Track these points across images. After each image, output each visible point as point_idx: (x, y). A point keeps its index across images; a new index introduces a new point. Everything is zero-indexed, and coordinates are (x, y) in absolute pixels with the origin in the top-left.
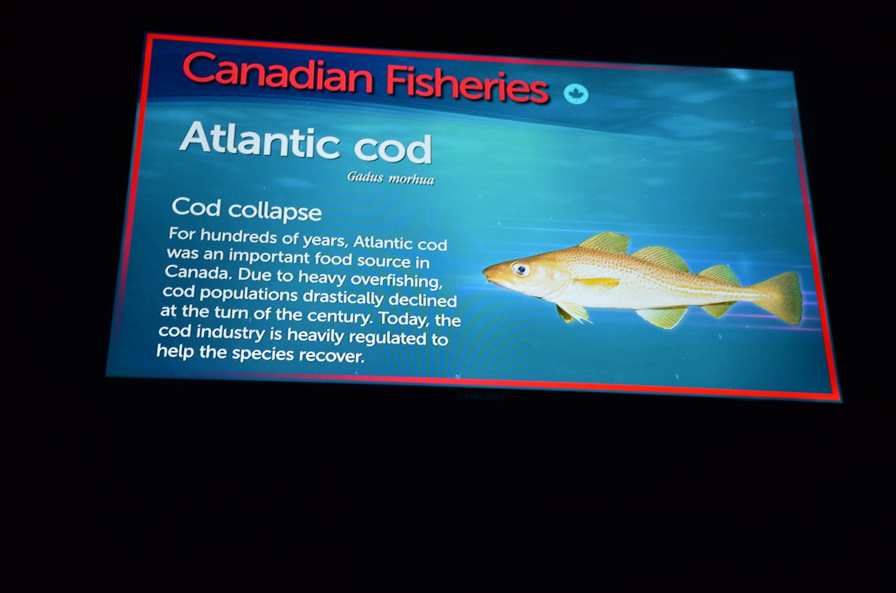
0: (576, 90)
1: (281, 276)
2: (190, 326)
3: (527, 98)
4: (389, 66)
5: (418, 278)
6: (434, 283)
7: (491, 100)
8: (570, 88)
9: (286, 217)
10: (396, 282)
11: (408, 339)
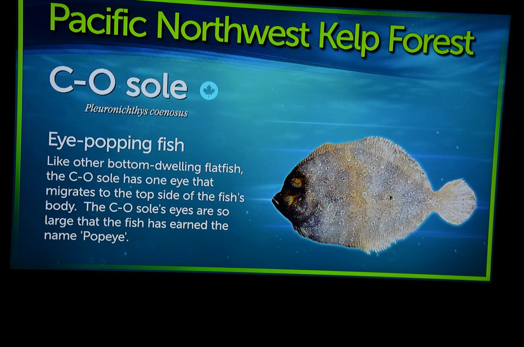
0: (209, 87)
1: (139, 194)
4: (52, 4)
6: (198, 168)
11: (84, 192)
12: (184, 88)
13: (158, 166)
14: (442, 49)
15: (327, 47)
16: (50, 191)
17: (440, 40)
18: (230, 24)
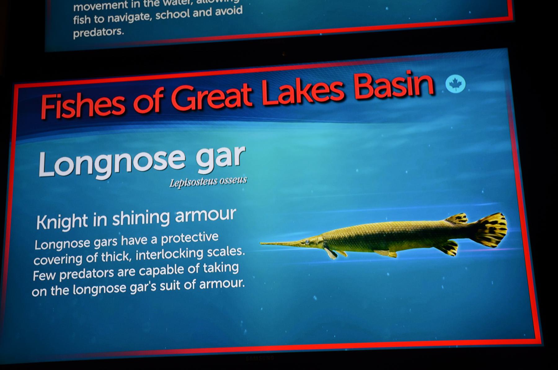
0: (455, 80)
2: (211, 8)
3: (327, 98)
7: (301, 103)
8: (450, 79)
9: (84, 273)
10: (80, 21)
12: (182, 158)
14: (320, 96)
15: (305, 101)
16: (77, 8)
17: (214, 95)
18: (82, 99)
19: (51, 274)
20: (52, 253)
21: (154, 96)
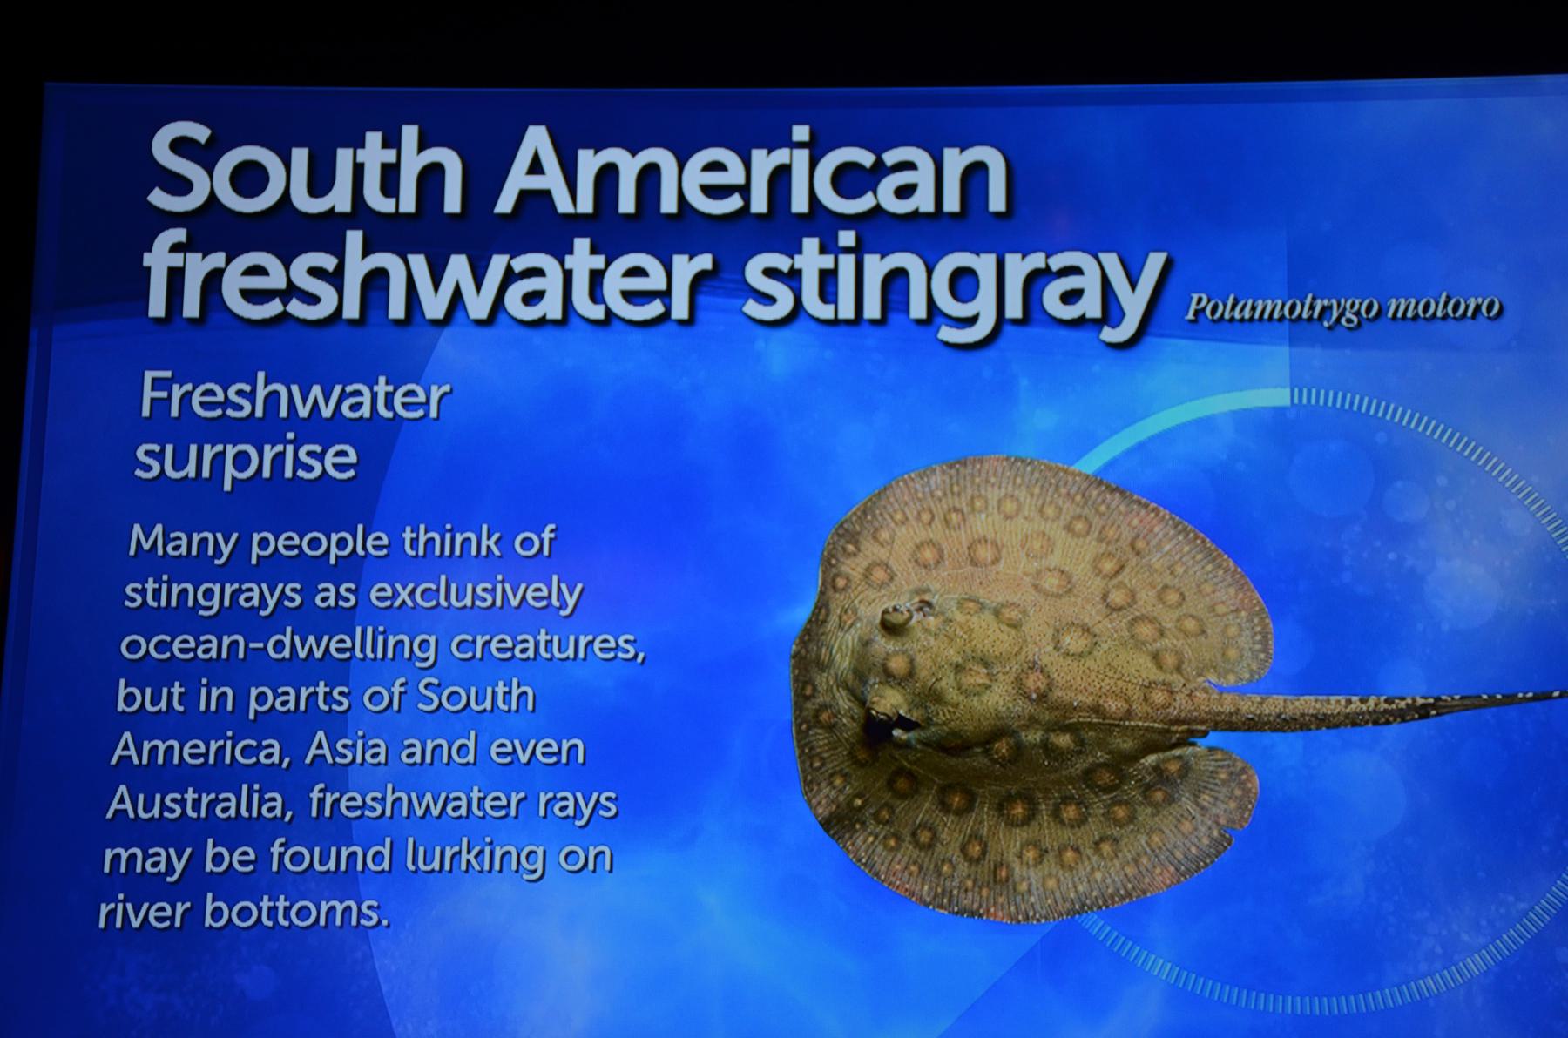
5: (858, 251)
13: (279, 646)
19: (316, 391)
20: (183, 618)
21: (570, 261)
